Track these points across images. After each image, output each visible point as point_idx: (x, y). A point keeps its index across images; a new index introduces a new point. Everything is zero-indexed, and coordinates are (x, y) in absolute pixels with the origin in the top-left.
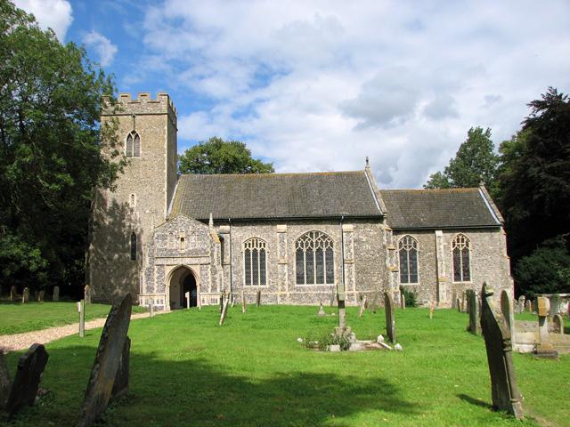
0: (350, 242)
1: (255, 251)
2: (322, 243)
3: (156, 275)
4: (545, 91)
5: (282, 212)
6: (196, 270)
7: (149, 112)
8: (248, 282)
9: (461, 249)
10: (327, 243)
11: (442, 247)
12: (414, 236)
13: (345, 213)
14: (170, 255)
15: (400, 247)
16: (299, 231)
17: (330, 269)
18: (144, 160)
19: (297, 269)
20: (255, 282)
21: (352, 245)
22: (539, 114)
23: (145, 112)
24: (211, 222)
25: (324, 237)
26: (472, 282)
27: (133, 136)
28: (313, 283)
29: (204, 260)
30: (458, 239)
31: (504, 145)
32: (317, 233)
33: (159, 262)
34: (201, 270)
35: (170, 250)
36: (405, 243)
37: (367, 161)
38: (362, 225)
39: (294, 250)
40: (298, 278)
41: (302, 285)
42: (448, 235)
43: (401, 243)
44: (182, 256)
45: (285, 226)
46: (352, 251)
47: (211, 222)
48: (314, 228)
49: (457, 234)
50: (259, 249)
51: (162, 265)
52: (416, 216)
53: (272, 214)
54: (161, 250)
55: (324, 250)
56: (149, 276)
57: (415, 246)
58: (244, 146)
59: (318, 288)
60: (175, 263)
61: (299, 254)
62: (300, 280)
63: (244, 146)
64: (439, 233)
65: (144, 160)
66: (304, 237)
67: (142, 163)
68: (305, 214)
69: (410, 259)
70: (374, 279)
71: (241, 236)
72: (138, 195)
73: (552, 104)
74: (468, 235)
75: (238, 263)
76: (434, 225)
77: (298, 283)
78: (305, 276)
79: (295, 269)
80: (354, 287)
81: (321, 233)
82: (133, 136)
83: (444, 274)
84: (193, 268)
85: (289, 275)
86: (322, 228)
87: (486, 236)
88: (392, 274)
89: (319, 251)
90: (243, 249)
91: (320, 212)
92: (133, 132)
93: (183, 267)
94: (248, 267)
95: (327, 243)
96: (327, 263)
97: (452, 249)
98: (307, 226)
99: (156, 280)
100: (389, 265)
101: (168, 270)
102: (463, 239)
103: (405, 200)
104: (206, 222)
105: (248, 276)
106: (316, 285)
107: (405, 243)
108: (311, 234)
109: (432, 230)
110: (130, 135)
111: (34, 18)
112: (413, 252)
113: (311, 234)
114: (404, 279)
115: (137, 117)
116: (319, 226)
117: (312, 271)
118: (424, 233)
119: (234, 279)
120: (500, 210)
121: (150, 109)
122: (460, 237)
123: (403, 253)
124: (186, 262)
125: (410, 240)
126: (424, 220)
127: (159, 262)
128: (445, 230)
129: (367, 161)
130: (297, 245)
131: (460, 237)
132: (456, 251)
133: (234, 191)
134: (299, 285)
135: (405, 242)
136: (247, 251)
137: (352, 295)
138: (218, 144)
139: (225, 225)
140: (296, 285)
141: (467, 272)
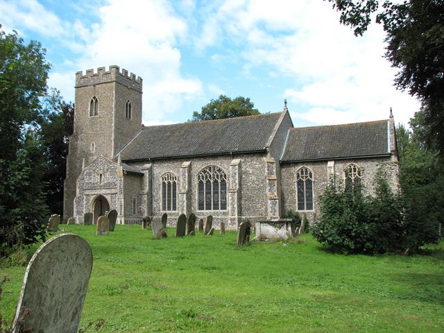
0: (235, 174)
1: (169, 183)
2: (203, 176)
3: (85, 202)
6: (108, 198)
7: (104, 81)
9: (353, 178)
10: (221, 176)
12: (310, 168)
15: (298, 177)
17: (224, 198)
18: (100, 117)
19: (199, 197)
20: (209, 208)
23: (102, 81)
25: (219, 170)
26: (314, 211)
28: (218, 209)
29: (113, 191)
32: (214, 167)
33: (87, 192)
34: (112, 198)
35: (93, 184)
36: (302, 173)
37: (286, 103)
38: (249, 160)
41: (202, 211)
43: (298, 174)
44: (101, 188)
48: (212, 163)
49: (348, 164)
50: (171, 182)
51: (88, 195)
54: (88, 184)
56: (79, 203)
57: (311, 176)
58: (248, 100)
60: (96, 193)
65: (100, 117)
69: (306, 188)
70: (259, 206)
75: (157, 193)
76: (327, 156)
77: (200, 209)
78: (205, 203)
82: (94, 101)
88: (269, 202)
89: (216, 182)
90: (161, 181)
92: (94, 98)
94: (164, 197)
95: (221, 176)
96: (221, 192)
99: (85, 206)
100: (268, 193)
101: (92, 198)
102: (355, 169)
105: (164, 204)
106: (212, 211)
109: (325, 161)
110: (92, 101)
112: (309, 182)
115: (97, 86)
117: (210, 199)
118: (177, 161)
121: (105, 79)
122: (352, 167)
123: (300, 183)
124: (102, 192)
125: (355, 169)
126: (320, 154)
127: (87, 192)
128: (336, 160)
129: (286, 103)
130: (199, 178)
131: (352, 167)
134: (200, 211)
135: (302, 173)
136: (164, 183)
137: (234, 219)
138: (225, 100)
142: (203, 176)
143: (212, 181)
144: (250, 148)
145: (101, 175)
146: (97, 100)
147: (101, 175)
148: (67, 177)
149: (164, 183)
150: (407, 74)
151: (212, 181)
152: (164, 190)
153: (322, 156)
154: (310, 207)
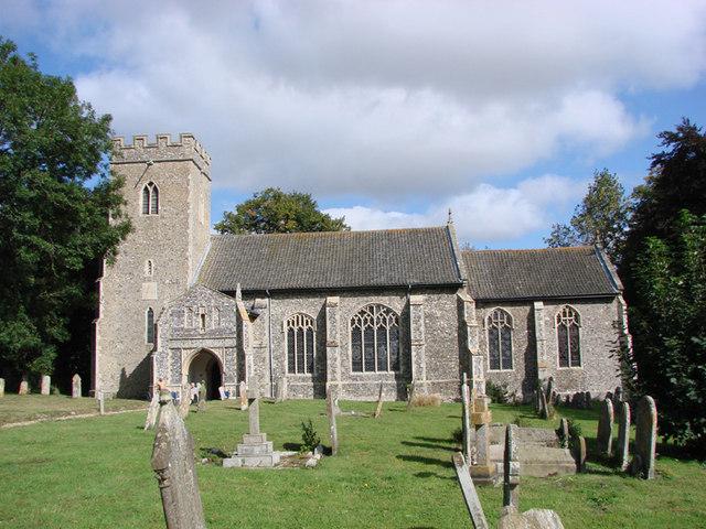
0: (420, 317)
2: (359, 320)
4: (680, 123)
5: (335, 280)
7: (169, 158)
8: (292, 370)
11: (542, 323)
13: (412, 281)
14: (187, 336)
15: (559, 320)
16: (356, 304)
21: (422, 321)
22: (669, 149)
24: (239, 293)
27: (151, 189)
30: (564, 313)
31: (638, 192)
32: (378, 306)
36: (565, 316)
38: (435, 297)
39: (350, 329)
40: (354, 363)
42: (551, 307)
45: (267, 300)
46: (422, 329)
47: (239, 293)
48: (374, 300)
50: (305, 328)
52: (516, 283)
53: (323, 284)
55: (363, 329)
58: (308, 197)
59: (380, 377)
61: (356, 333)
62: (357, 366)
63: (308, 197)
64: (538, 305)
66: (362, 313)
67: (160, 222)
68: (363, 283)
71: (283, 313)
72: (155, 261)
73: (686, 138)
74: (577, 307)
77: (354, 370)
79: (350, 352)
80: (424, 375)
81: (384, 307)
82: (151, 189)
83: (545, 358)
84: (216, 352)
85: (343, 361)
86: (385, 300)
87: (600, 308)
91: (382, 280)
92: (151, 184)
93: (204, 351)
97: (557, 325)
98: (365, 298)
103: (502, 262)
104: (232, 294)
105: (291, 363)
107: (565, 316)
108: (371, 309)
110: (146, 189)
111: (87, 396)
113: (371, 309)
114: (495, 365)
116: (380, 298)
119: (274, 366)
120: (98, 299)
121: (170, 155)
122: (567, 310)
124: (207, 344)
126: (521, 292)
128: (548, 300)
131: (567, 310)
132: (562, 328)
133: (286, 255)
136: (291, 330)
139: (263, 298)
140: (352, 373)
141: (576, 354)
142: (359, 320)
143: (376, 328)
144: (439, 279)
145: (203, 316)
146: (155, 189)
147: (203, 316)
148: (101, 316)
149: (291, 330)
150: (646, 195)
151: (376, 328)
152: (291, 342)
153: (525, 295)
154: (508, 365)
